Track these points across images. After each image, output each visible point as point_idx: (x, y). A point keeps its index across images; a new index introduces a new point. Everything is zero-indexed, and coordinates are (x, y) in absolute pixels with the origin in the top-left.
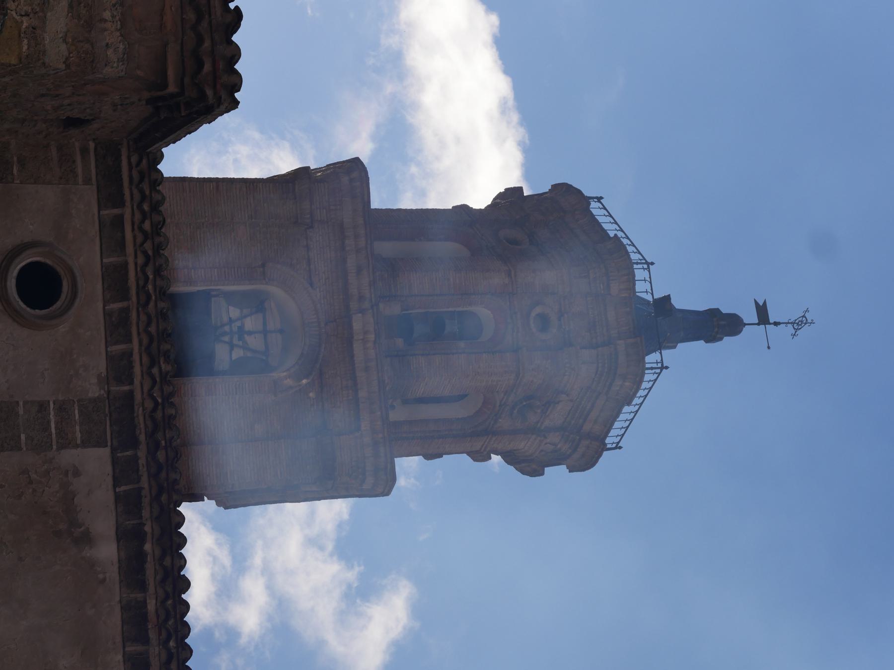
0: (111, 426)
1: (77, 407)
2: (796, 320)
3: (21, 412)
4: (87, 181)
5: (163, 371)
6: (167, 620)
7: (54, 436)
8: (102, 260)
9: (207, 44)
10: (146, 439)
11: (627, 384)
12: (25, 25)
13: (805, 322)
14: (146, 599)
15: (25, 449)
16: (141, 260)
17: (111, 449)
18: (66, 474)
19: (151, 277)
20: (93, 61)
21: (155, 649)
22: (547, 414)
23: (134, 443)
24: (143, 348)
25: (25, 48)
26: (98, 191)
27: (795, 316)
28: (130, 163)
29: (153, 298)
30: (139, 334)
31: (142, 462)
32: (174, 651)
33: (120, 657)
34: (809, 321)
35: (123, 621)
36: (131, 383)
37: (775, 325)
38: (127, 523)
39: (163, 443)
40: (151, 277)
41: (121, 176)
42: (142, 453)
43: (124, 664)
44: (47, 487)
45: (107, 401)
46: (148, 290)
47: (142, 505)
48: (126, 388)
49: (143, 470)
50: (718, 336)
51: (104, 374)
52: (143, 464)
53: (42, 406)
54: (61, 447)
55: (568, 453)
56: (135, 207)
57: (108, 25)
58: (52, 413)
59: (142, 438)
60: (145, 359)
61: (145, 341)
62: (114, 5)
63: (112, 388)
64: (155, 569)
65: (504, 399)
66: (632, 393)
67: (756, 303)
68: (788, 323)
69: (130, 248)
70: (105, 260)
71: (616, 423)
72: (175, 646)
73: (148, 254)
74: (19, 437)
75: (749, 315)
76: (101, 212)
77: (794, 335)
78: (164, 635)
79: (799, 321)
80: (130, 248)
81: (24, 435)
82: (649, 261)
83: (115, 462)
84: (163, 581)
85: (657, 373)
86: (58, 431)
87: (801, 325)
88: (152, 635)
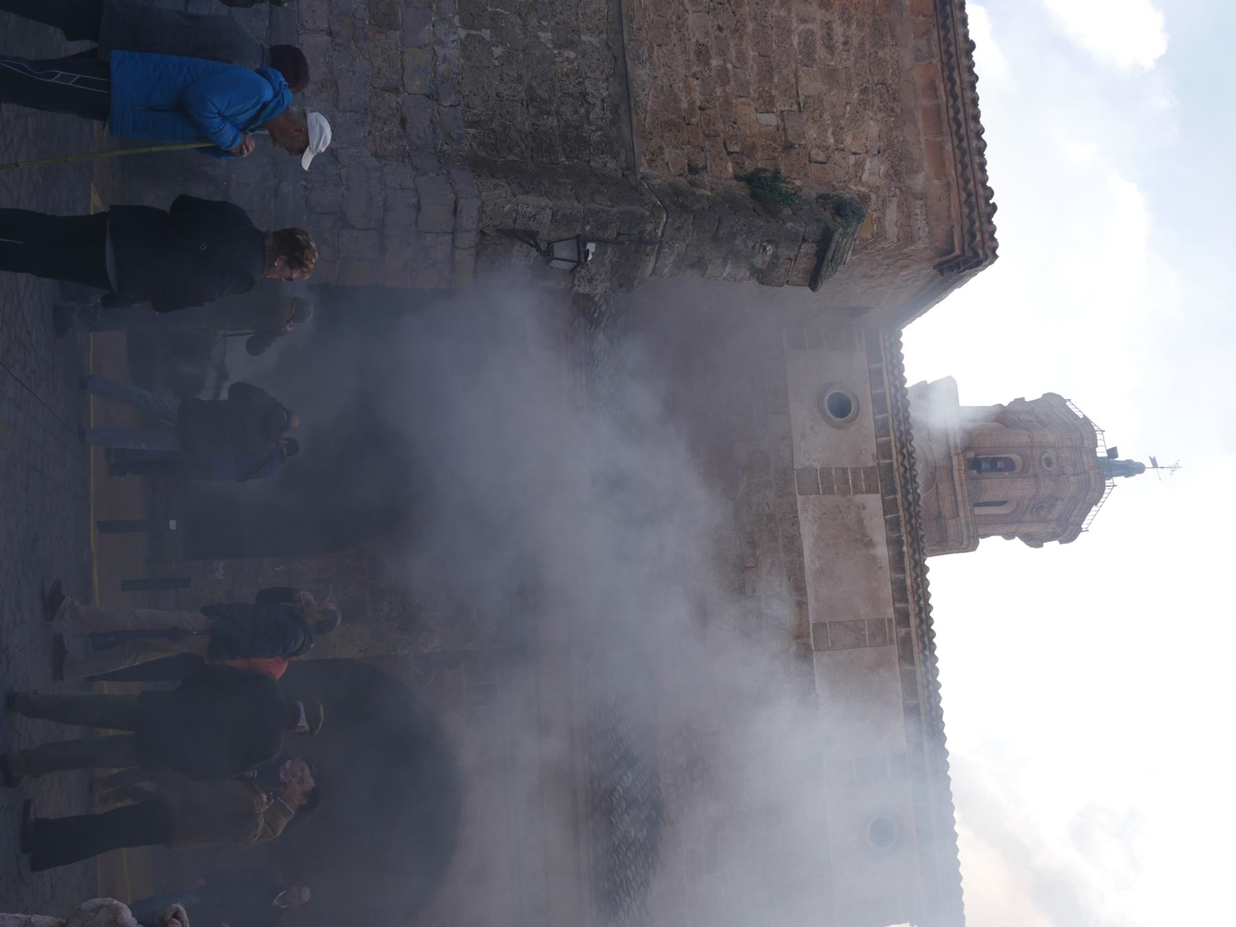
0: (881, 482)
3: (834, 474)
6: (918, 589)
9: (977, 224)
12: (875, 216)
18: (859, 508)
20: (912, 237)
23: (894, 492)
24: (897, 439)
25: (876, 228)
30: (894, 431)
31: (899, 501)
32: (923, 606)
33: (892, 610)
35: (892, 590)
36: (891, 457)
39: (911, 491)
40: (900, 399)
42: (899, 496)
48: (889, 461)
53: (844, 471)
54: (855, 493)
57: (919, 217)
58: (850, 474)
59: (899, 488)
62: (922, 206)
67: (1150, 458)
70: (873, 392)
75: (1148, 464)
78: (916, 598)
84: (915, 567)
88: (910, 598)
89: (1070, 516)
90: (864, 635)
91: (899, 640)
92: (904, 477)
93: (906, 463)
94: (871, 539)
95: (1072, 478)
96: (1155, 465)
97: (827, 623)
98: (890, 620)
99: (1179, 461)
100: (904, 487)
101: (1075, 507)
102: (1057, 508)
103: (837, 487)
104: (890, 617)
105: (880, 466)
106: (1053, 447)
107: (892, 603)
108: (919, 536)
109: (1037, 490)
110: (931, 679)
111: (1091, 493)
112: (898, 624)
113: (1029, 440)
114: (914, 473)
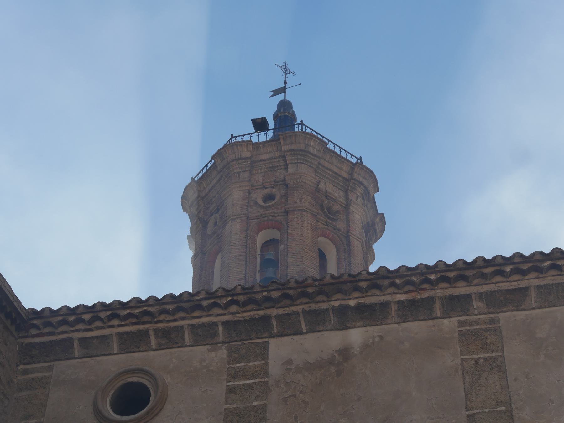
0: (251, 339)
1: (234, 365)
2: (283, 72)
3: (235, 406)
4: (50, 369)
5: (205, 296)
7: (256, 380)
8: (116, 354)
10: (263, 309)
11: (312, 144)
13: (285, 67)
14: (396, 302)
15: (265, 402)
16: (115, 322)
17: (270, 338)
18: (290, 369)
19: (128, 311)
21: (438, 292)
22: (335, 198)
23: (266, 319)
26: (59, 360)
27: (280, 73)
28: (37, 336)
29: (145, 308)
30: (175, 320)
31: (281, 311)
32: (439, 275)
33: (446, 321)
34: (285, 64)
36: (216, 324)
37: (286, 84)
38: (332, 321)
39: (265, 294)
40: (128, 311)
41: (47, 342)
42: (274, 312)
43: (451, 317)
44: (298, 384)
45: (231, 344)
46: (139, 312)
47: (317, 309)
48: (220, 328)
49: (288, 310)
50: (291, 112)
51: (208, 347)
52: (283, 311)
53: (231, 390)
54: (266, 375)
55: (364, 188)
56: (72, 329)
59: (261, 313)
60: (196, 314)
61: (182, 314)
63: (220, 340)
64: (371, 296)
65: (323, 222)
66: (319, 141)
68: (285, 76)
69: (107, 332)
71: (341, 155)
72: (434, 275)
73: (110, 314)
74: (255, 406)
76: (75, 356)
77: (293, 74)
79: (284, 70)
80: (107, 332)
81: (253, 402)
82: (230, 137)
83: (281, 335)
85: (306, 128)
86: (253, 378)
87: (287, 69)
88: (426, 295)
89: (340, 176)
90: (485, 359)
91: (491, 310)
92: (244, 304)
93: (224, 301)
94: (336, 351)
95: (290, 170)
96: (283, 90)
97: (468, 413)
98: (461, 324)
99: (277, 65)
100: (258, 304)
101: (329, 170)
102: (329, 190)
103: (256, 400)
104: (456, 324)
105: (227, 340)
106: (249, 193)
107: (435, 321)
108: (334, 281)
109: (305, 211)
110: (547, 263)
111: (311, 149)
112: (466, 311)
113: (238, 221)
114: (239, 290)
